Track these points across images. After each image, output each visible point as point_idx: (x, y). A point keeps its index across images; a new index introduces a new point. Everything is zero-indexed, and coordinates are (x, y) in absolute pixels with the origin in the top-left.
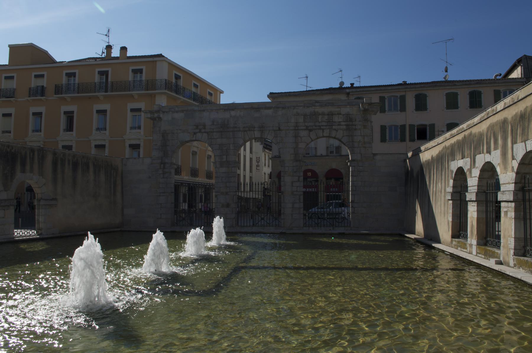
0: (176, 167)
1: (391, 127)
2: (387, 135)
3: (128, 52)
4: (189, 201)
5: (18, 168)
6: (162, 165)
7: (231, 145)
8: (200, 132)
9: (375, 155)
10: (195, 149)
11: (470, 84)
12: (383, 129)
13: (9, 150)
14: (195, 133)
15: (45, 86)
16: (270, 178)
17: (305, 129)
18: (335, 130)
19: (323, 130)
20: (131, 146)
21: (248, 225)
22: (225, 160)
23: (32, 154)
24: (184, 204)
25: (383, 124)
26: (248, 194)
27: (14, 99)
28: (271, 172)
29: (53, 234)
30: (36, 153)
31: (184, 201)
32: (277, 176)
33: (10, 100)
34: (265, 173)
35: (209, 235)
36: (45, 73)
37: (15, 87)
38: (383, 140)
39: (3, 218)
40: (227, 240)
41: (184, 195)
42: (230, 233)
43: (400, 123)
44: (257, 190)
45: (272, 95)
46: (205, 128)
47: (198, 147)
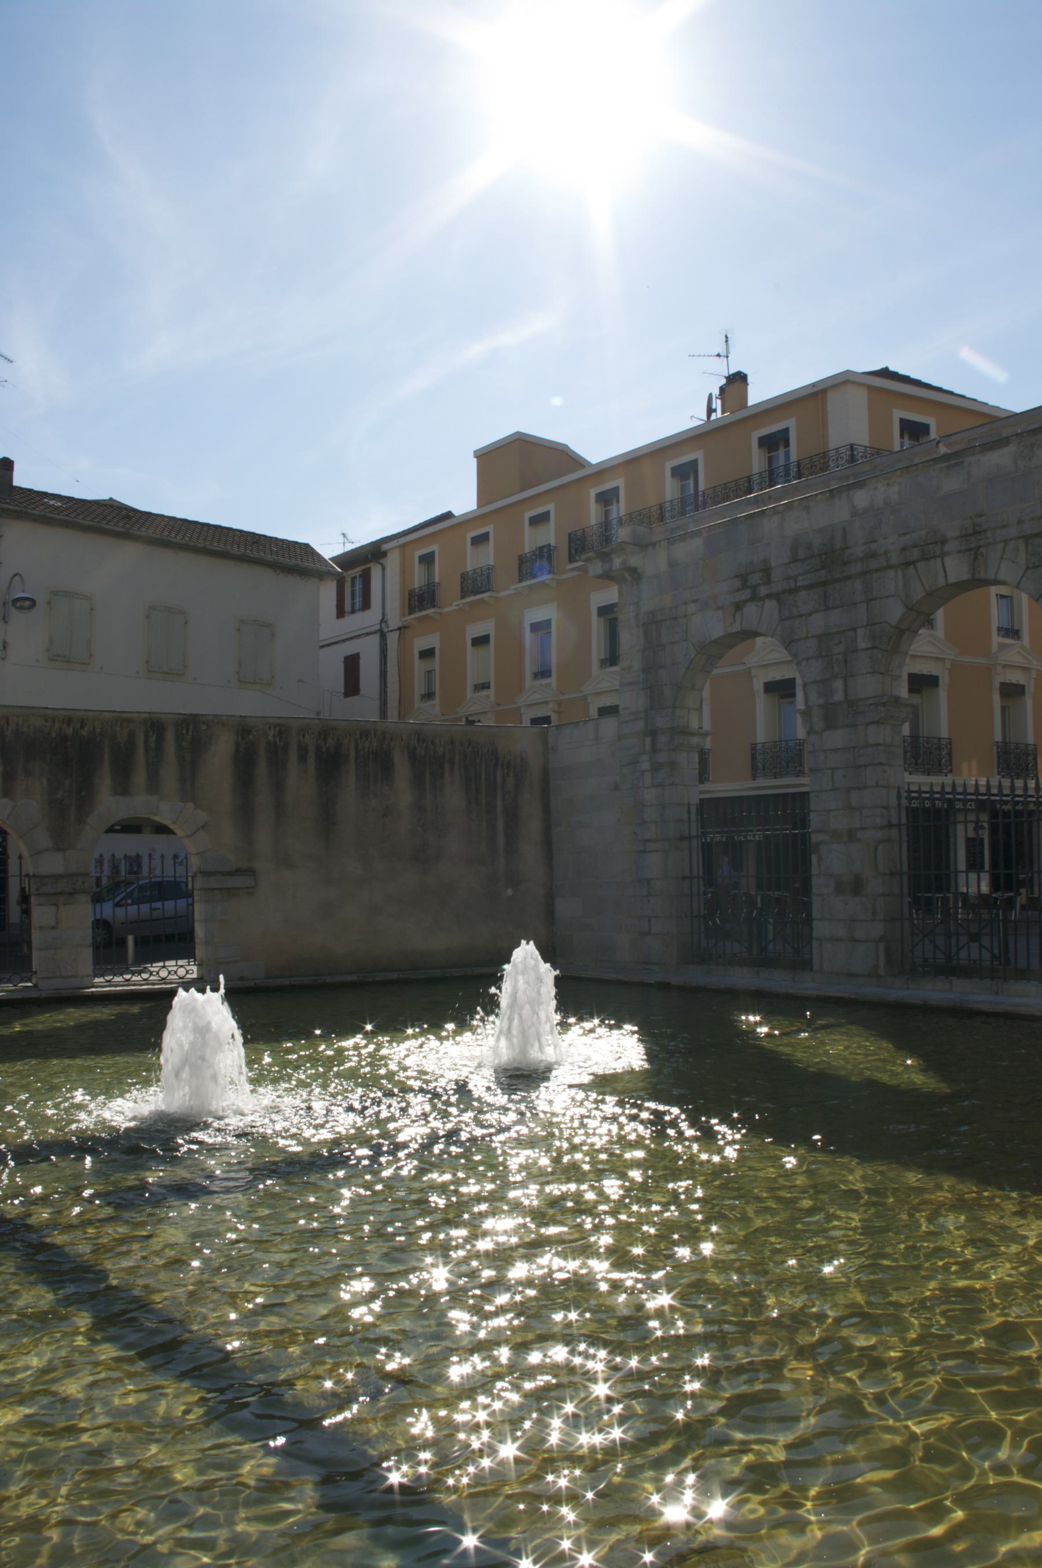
3: (751, 389)
4: (994, 864)
5: (104, 781)
6: (648, 740)
7: (860, 632)
8: (754, 598)
10: (1015, 677)
13: (70, 731)
14: (738, 607)
15: (553, 544)
20: (770, 687)
22: (839, 697)
23: (153, 739)
24: (973, 876)
27: (488, 594)
29: (241, 979)
30: (170, 736)
31: (974, 864)
33: (482, 601)
36: (550, 507)
37: (492, 563)
39: (53, 928)
41: (973, 846)
46: (768, 581)
47: (1026, 669)
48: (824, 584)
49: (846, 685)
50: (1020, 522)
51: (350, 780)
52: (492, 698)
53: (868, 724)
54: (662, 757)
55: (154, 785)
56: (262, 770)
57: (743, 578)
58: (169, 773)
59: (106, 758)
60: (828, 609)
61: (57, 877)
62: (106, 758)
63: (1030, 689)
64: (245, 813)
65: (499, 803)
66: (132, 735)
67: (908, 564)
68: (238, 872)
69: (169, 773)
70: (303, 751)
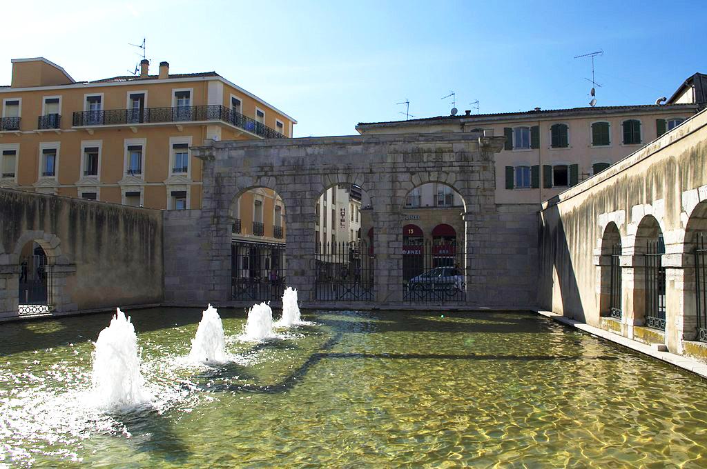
1: (519, 169)
4: (250, 267)
6: (216, 220)
7: (307, 193)
10: (259, 198)
12: (509, 170)
14: (259, 177)
16: (359, 237)
17: (405, 172)
19: (429, 172)
20: (174, 194)
22: (299, 212)
26: (330, 258)
27: (18, 131)
30: (48, 204)
31: (245, 267)
32: (367, 234)
34: (352, 230)
35: (277, 312)
37: (20, 116)
38: (509, 185)
39: (4, 289)
41: (245, 259)
42: (306, 310)
45: (361, 126)
48: (295, 175)
49: (301, 209)
50: (363, 168)
51: (106, 227)
52: (16, 182)
53: (309, 222)
54: (221, 226)
55: (42, 227)
56: (79, 222)
57: (262, 168)
58: (48, 220)
59: (25, 212)
60: (295, 183)
61: (7, 266)
62: (25, 212)
63: (263, 204)
64: (73, 239)
65: (149, 239)
66: (34, 203)
67: (325, 174)
68: (70, 265)
69: (48, 220)
70: (92, 214)
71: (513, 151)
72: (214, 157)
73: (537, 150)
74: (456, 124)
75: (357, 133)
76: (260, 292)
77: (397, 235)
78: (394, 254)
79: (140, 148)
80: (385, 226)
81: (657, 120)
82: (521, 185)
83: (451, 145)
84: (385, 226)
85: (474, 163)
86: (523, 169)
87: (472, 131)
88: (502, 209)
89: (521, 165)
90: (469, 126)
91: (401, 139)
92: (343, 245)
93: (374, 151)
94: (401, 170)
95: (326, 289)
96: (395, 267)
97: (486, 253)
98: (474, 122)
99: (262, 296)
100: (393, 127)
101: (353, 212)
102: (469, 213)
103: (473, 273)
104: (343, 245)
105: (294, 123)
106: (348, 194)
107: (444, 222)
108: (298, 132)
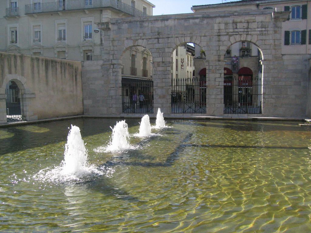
0: (122, 67)
1: (293, 32)
2: (290, 39)
9: (283, 55)
11: (209, 8)
12: (287, 33)
16: (194, 75)
17: (225, 35)
18: (251, 35)
19: (241, 35)
21: (175, 112)
25: (287, 30)
26: (175, 88)
28: (194, 71)
32: (202, 74)
34: (188, 72)
35: (153, 120)
38: (287, 43)
40: (166, 124)
42: (167, 119)
43: (302, 29)
44: (182, 85)
45: (195, 8)
58: (19, 68)
71: (290, 21)
72: (110, 28)
73: (305, 20)
74: (253, 5)
75: (192, 12)
76: (137, 108)
77: (221, 74)
78: (219, 85)
79: (92, 21)
80: (214, 69)
81: (285, 7)
82: (294, 43)
83: (254, 17)
84: (214, 69)
85: (269, 29)
86: (295, 32)
87: (264, 9)
88: (285, 58)
89: (294, 30)
90: (261, 6)
91: (198, 16)
92: (183, 80)
93: (206, 22)
94: (223, 34)
95: (175, 106)
96: (219, 93)
97: (275, 84)
98: (265, 3)
99: (138, 111)
100: (214, 8)
101: (188, 60)
102: (265, 60)
103: (266, 96)
104: (183, 80)
105: (154, 6)
106: (185, 50)
107: (245, 66)
108: (156, 12)
